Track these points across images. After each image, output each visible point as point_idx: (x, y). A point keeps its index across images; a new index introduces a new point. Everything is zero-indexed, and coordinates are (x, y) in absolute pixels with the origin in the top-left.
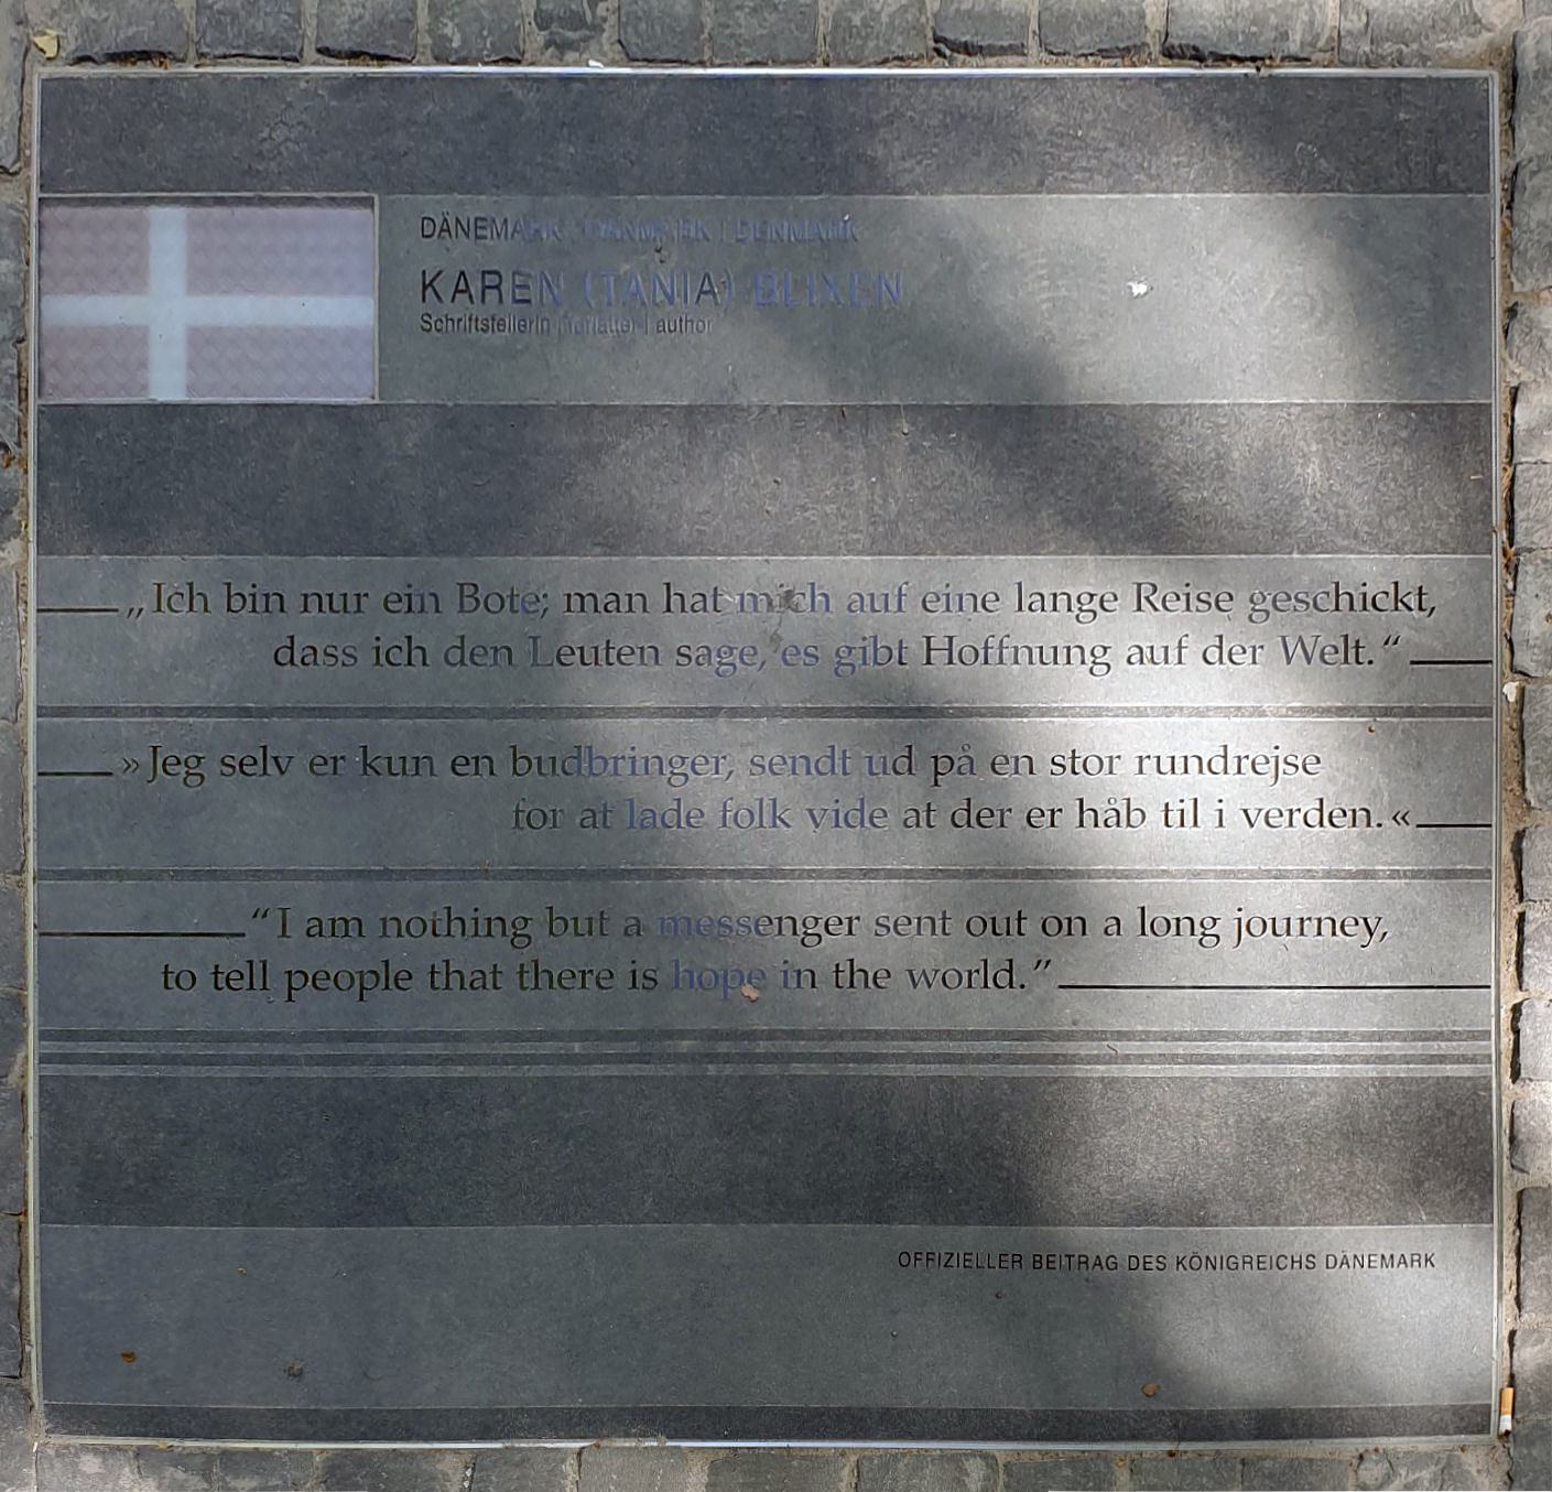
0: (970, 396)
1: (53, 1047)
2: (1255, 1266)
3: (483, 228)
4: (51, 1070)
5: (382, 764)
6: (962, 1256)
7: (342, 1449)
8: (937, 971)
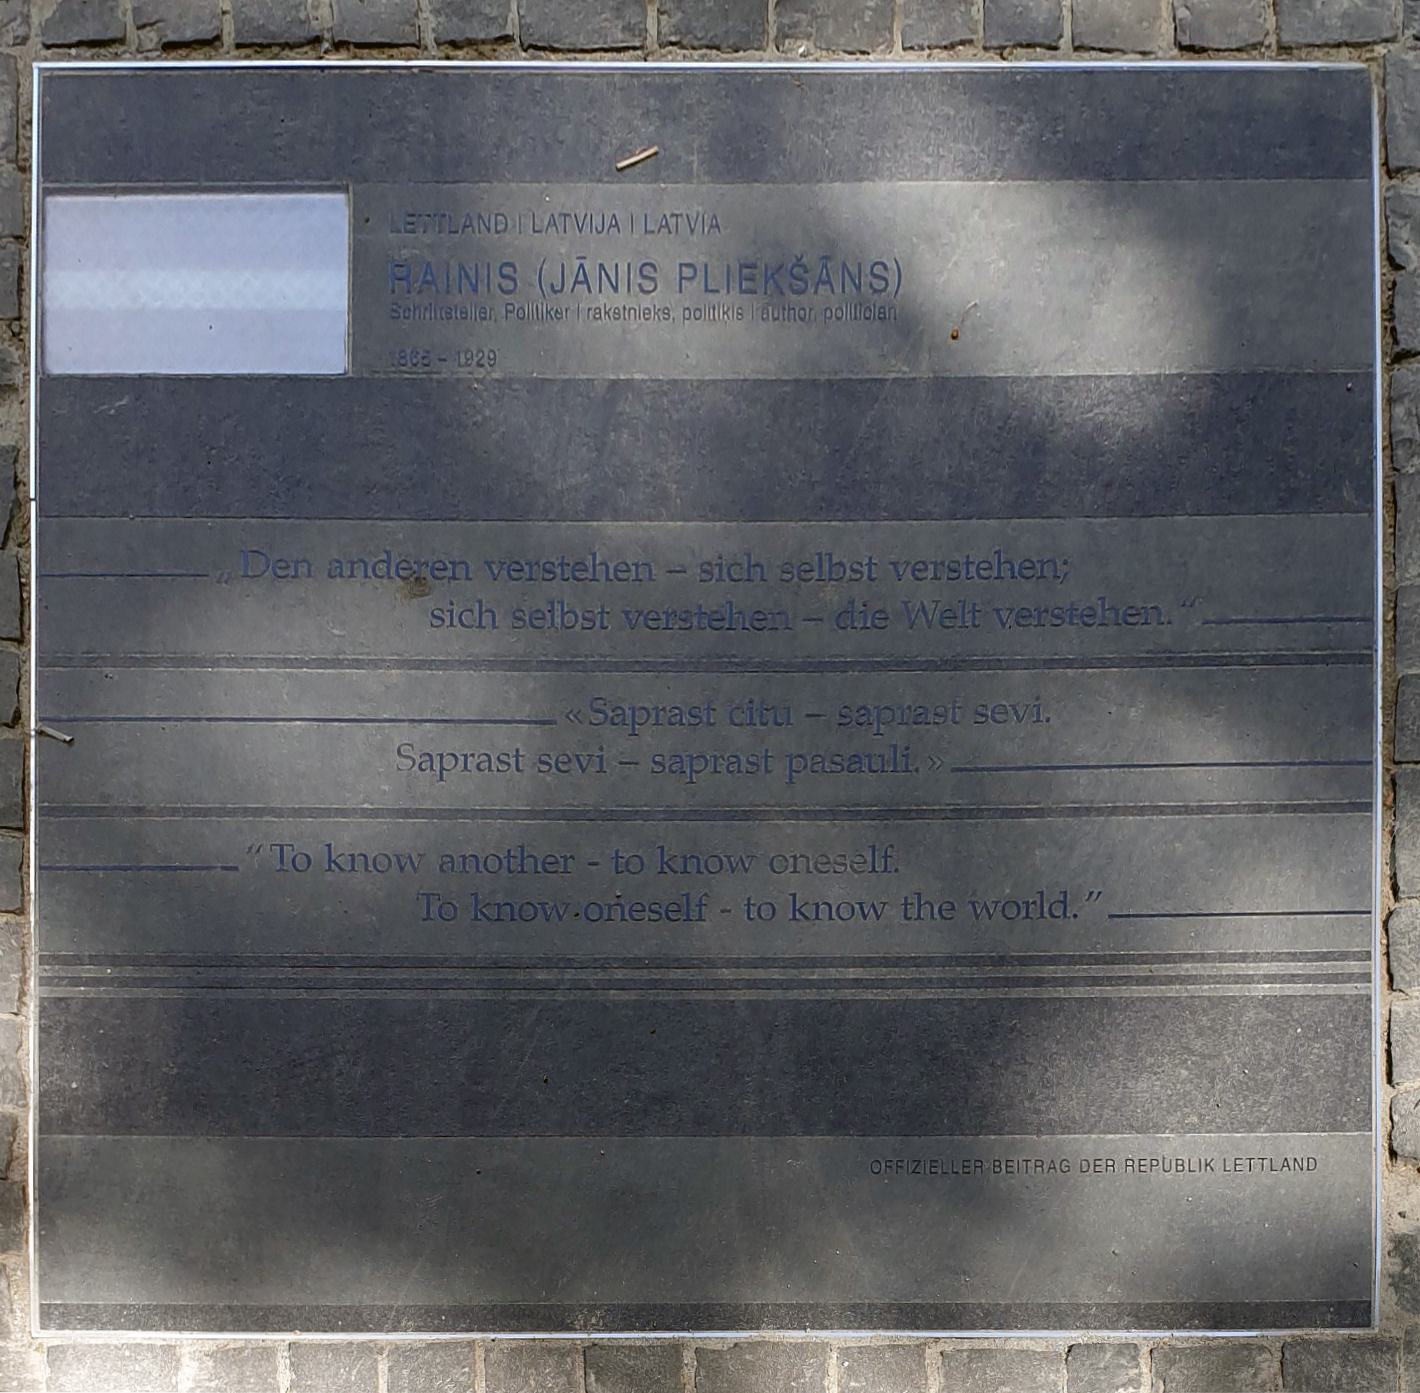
0: (905, 369)
2: (1136, 1169)
8: (997, 903)
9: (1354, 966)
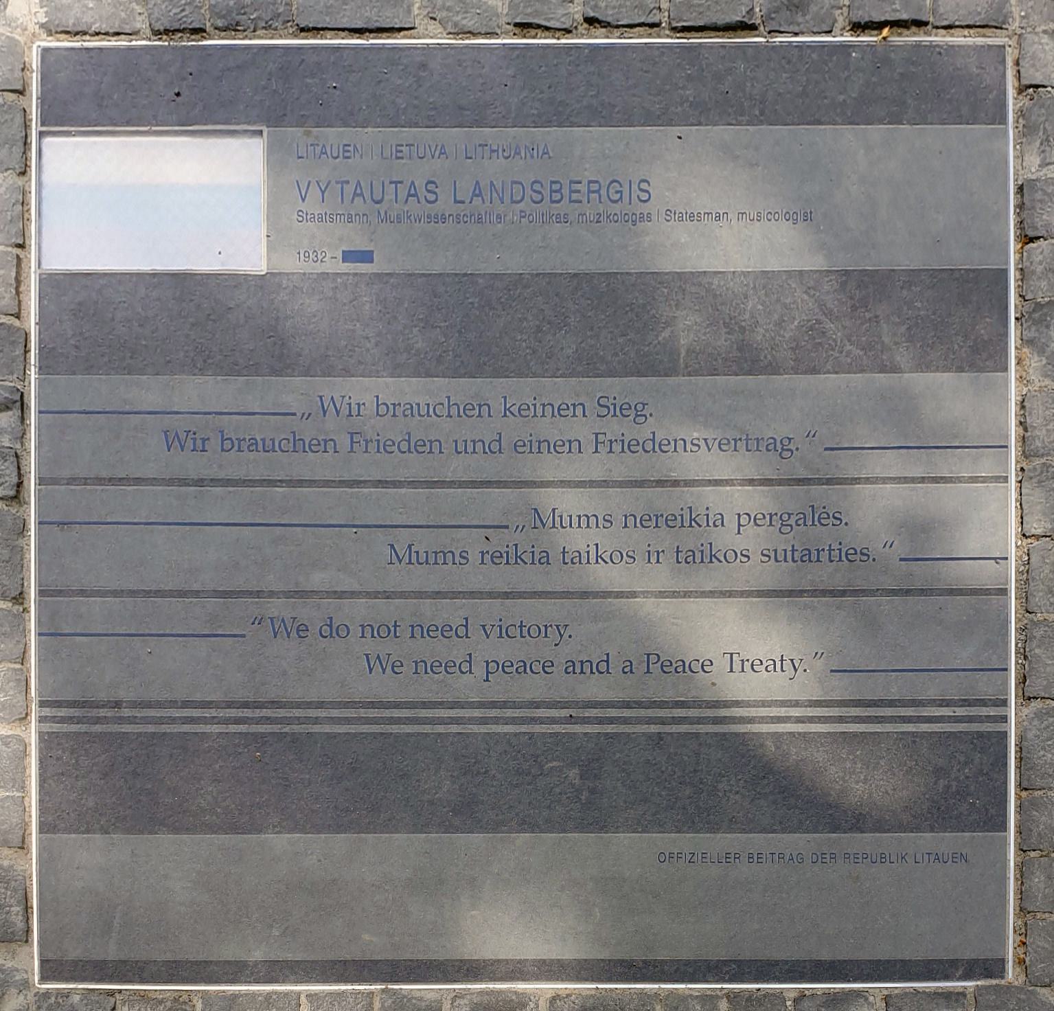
1: (47, 712)
3: (349, 151)
4: (47, 727)
5: (606, 557)
6: (950, 855)
7: (284, 982)
9: (992, 712)
